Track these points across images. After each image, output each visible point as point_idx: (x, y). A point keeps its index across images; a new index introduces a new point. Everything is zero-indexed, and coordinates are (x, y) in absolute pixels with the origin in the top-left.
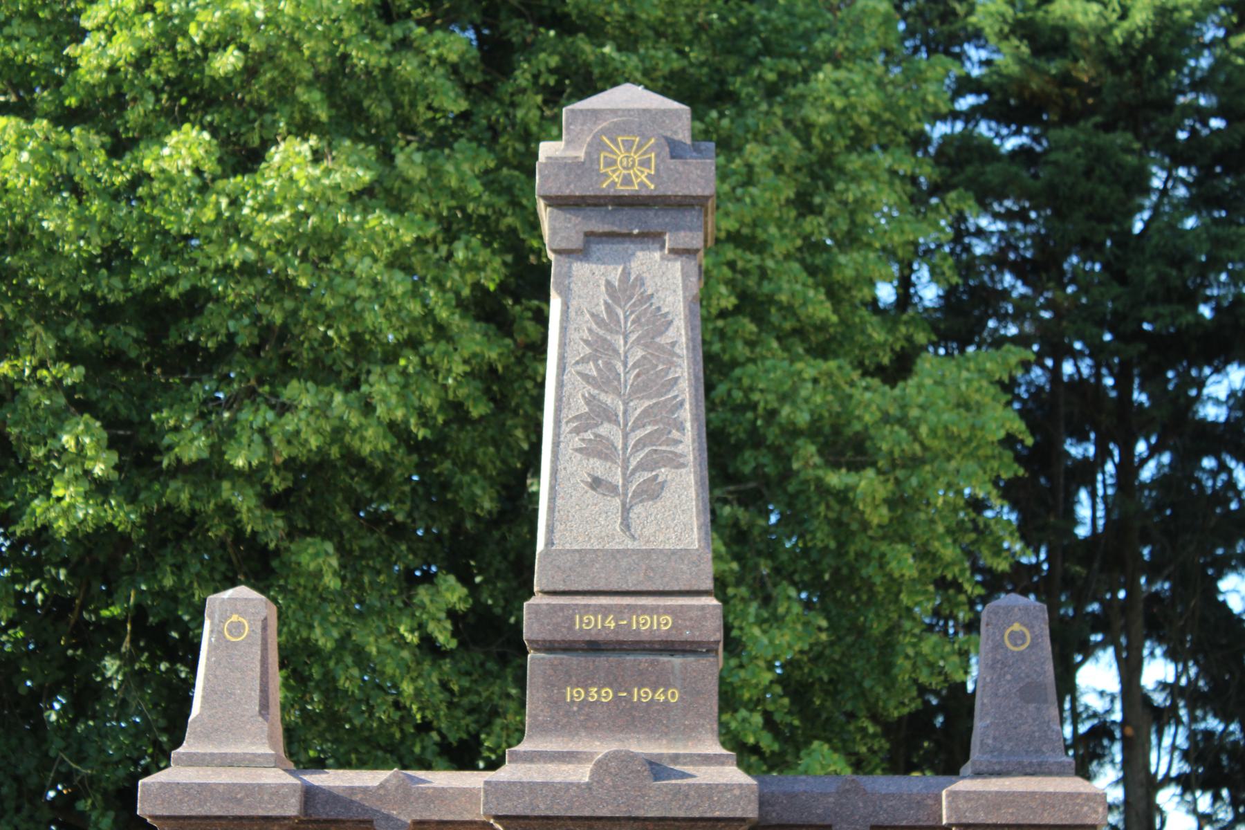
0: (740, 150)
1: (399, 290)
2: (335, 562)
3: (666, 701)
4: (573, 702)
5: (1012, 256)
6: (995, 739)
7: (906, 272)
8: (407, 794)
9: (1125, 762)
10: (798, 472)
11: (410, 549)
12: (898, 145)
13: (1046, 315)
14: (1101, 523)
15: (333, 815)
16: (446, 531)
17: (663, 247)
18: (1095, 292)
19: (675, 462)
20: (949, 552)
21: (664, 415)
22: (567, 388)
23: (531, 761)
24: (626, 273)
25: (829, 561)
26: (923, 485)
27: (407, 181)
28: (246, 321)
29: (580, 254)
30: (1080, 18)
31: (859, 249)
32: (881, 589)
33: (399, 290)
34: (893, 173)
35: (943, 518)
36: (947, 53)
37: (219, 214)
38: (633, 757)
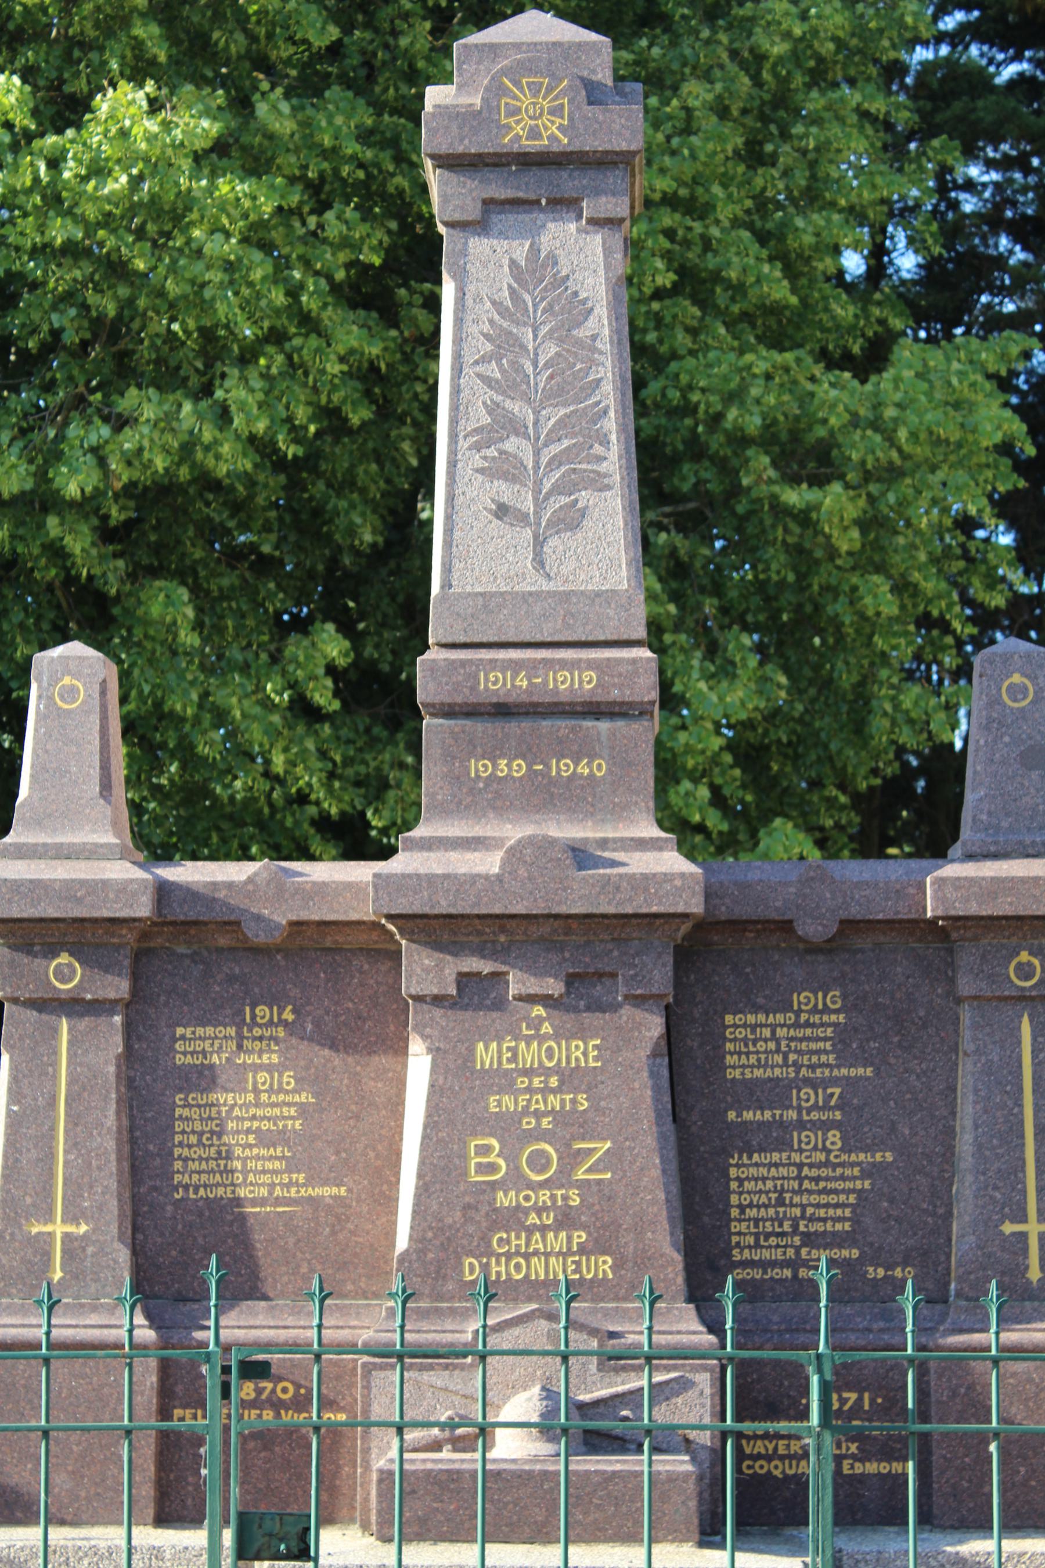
0: (675, 88)
1: (257, 275)
2: (190, 612)
3: (591, 775)
4: (478, 777)
5: (1009, 214)
6: (990, 814)
8: (281, 889)
10: (749, 489)
11: (279, 586)
12: (869, 79)
15: (192, 916)
16: (320, 567)
17: (579, 217)
19: (598, 483)
22: (465, 394)
23: (430, 849)
24: (535, 250)
25: (788, 598)
26: (903, 503)
27: (270, 136)
28: (73, 312)
29: (479, 226)
31: (822, 208)
32: (851, 631)
33: (257, 275)
34: (864, 115)
37: (36, 180)
38: (553, 842)
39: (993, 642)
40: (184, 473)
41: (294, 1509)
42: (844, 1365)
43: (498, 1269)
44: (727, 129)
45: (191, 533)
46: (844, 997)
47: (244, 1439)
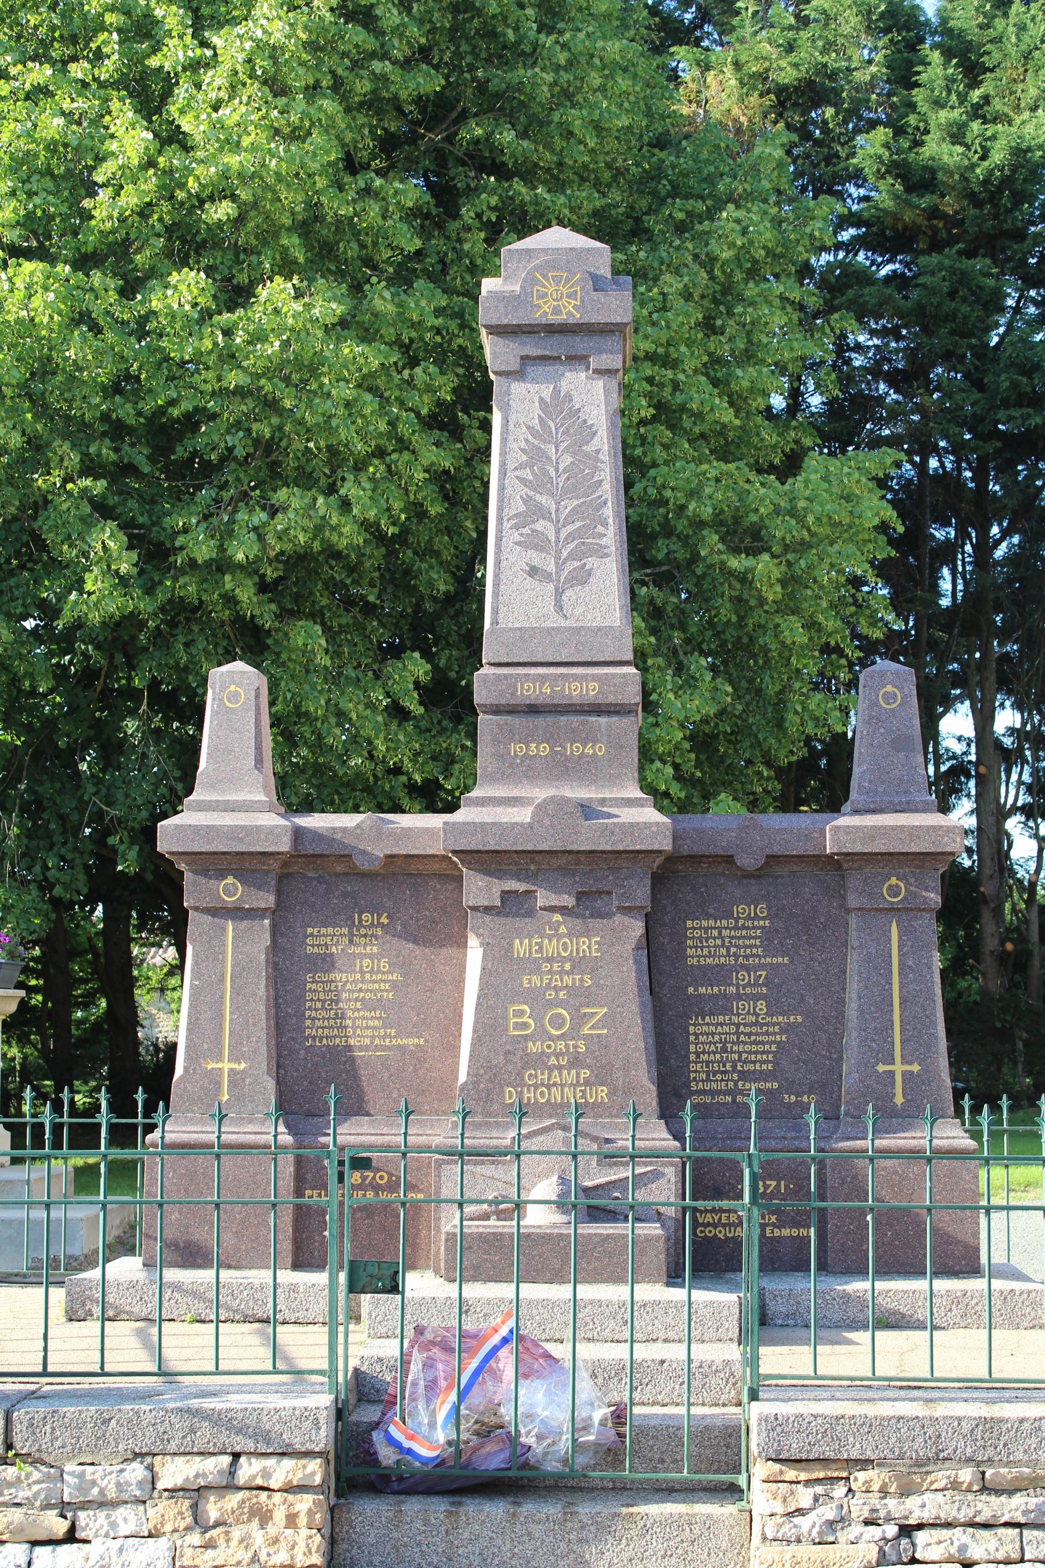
0: (656, 279)
3: (595, 754)
7: (796, 384)
8: (380, 832)
9: (978, 795)
12: (789, 275)
13: (916, 418)
14: (960, 595)
15: (318, 851)
17: (588, 368)
18: (958, 397)
19: (601, 552)
20: (831, 623)
21: (591, 512)
24: (556, 391)
29: (518, 375)
30: (946, 158)
33: (367, 411)
34: (783, 298)
35: (827, 594)
36: (831, 192)
37: (216, 344)
38: (568, 800)
39: (874, 663)
40: (317, 546)
41: (388, 1258)
42: (767, 1162)
43: (528, 1095)
44: (690, 307)
45: (320, 586)
46: (769, 908)
47: (354, 1211)
